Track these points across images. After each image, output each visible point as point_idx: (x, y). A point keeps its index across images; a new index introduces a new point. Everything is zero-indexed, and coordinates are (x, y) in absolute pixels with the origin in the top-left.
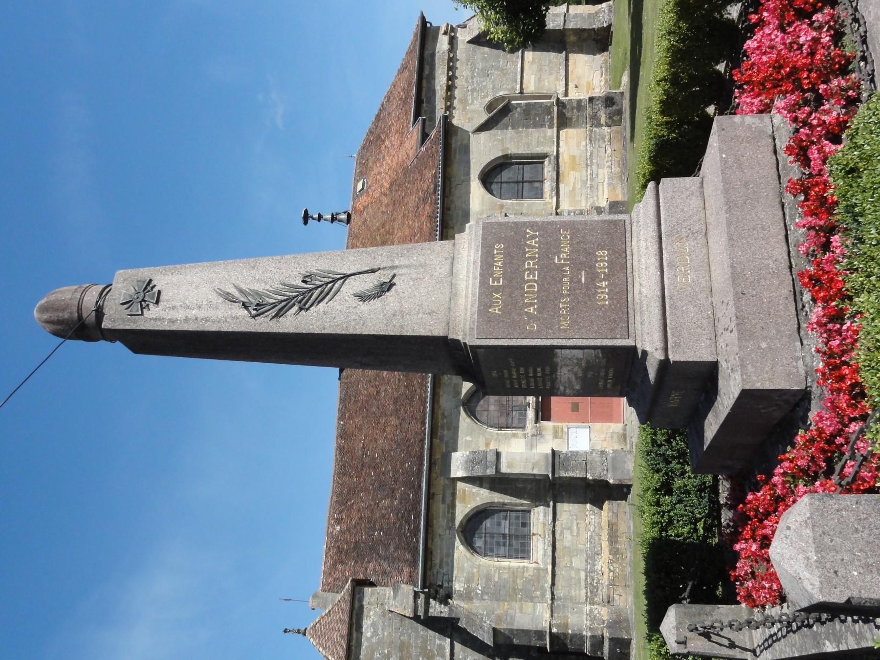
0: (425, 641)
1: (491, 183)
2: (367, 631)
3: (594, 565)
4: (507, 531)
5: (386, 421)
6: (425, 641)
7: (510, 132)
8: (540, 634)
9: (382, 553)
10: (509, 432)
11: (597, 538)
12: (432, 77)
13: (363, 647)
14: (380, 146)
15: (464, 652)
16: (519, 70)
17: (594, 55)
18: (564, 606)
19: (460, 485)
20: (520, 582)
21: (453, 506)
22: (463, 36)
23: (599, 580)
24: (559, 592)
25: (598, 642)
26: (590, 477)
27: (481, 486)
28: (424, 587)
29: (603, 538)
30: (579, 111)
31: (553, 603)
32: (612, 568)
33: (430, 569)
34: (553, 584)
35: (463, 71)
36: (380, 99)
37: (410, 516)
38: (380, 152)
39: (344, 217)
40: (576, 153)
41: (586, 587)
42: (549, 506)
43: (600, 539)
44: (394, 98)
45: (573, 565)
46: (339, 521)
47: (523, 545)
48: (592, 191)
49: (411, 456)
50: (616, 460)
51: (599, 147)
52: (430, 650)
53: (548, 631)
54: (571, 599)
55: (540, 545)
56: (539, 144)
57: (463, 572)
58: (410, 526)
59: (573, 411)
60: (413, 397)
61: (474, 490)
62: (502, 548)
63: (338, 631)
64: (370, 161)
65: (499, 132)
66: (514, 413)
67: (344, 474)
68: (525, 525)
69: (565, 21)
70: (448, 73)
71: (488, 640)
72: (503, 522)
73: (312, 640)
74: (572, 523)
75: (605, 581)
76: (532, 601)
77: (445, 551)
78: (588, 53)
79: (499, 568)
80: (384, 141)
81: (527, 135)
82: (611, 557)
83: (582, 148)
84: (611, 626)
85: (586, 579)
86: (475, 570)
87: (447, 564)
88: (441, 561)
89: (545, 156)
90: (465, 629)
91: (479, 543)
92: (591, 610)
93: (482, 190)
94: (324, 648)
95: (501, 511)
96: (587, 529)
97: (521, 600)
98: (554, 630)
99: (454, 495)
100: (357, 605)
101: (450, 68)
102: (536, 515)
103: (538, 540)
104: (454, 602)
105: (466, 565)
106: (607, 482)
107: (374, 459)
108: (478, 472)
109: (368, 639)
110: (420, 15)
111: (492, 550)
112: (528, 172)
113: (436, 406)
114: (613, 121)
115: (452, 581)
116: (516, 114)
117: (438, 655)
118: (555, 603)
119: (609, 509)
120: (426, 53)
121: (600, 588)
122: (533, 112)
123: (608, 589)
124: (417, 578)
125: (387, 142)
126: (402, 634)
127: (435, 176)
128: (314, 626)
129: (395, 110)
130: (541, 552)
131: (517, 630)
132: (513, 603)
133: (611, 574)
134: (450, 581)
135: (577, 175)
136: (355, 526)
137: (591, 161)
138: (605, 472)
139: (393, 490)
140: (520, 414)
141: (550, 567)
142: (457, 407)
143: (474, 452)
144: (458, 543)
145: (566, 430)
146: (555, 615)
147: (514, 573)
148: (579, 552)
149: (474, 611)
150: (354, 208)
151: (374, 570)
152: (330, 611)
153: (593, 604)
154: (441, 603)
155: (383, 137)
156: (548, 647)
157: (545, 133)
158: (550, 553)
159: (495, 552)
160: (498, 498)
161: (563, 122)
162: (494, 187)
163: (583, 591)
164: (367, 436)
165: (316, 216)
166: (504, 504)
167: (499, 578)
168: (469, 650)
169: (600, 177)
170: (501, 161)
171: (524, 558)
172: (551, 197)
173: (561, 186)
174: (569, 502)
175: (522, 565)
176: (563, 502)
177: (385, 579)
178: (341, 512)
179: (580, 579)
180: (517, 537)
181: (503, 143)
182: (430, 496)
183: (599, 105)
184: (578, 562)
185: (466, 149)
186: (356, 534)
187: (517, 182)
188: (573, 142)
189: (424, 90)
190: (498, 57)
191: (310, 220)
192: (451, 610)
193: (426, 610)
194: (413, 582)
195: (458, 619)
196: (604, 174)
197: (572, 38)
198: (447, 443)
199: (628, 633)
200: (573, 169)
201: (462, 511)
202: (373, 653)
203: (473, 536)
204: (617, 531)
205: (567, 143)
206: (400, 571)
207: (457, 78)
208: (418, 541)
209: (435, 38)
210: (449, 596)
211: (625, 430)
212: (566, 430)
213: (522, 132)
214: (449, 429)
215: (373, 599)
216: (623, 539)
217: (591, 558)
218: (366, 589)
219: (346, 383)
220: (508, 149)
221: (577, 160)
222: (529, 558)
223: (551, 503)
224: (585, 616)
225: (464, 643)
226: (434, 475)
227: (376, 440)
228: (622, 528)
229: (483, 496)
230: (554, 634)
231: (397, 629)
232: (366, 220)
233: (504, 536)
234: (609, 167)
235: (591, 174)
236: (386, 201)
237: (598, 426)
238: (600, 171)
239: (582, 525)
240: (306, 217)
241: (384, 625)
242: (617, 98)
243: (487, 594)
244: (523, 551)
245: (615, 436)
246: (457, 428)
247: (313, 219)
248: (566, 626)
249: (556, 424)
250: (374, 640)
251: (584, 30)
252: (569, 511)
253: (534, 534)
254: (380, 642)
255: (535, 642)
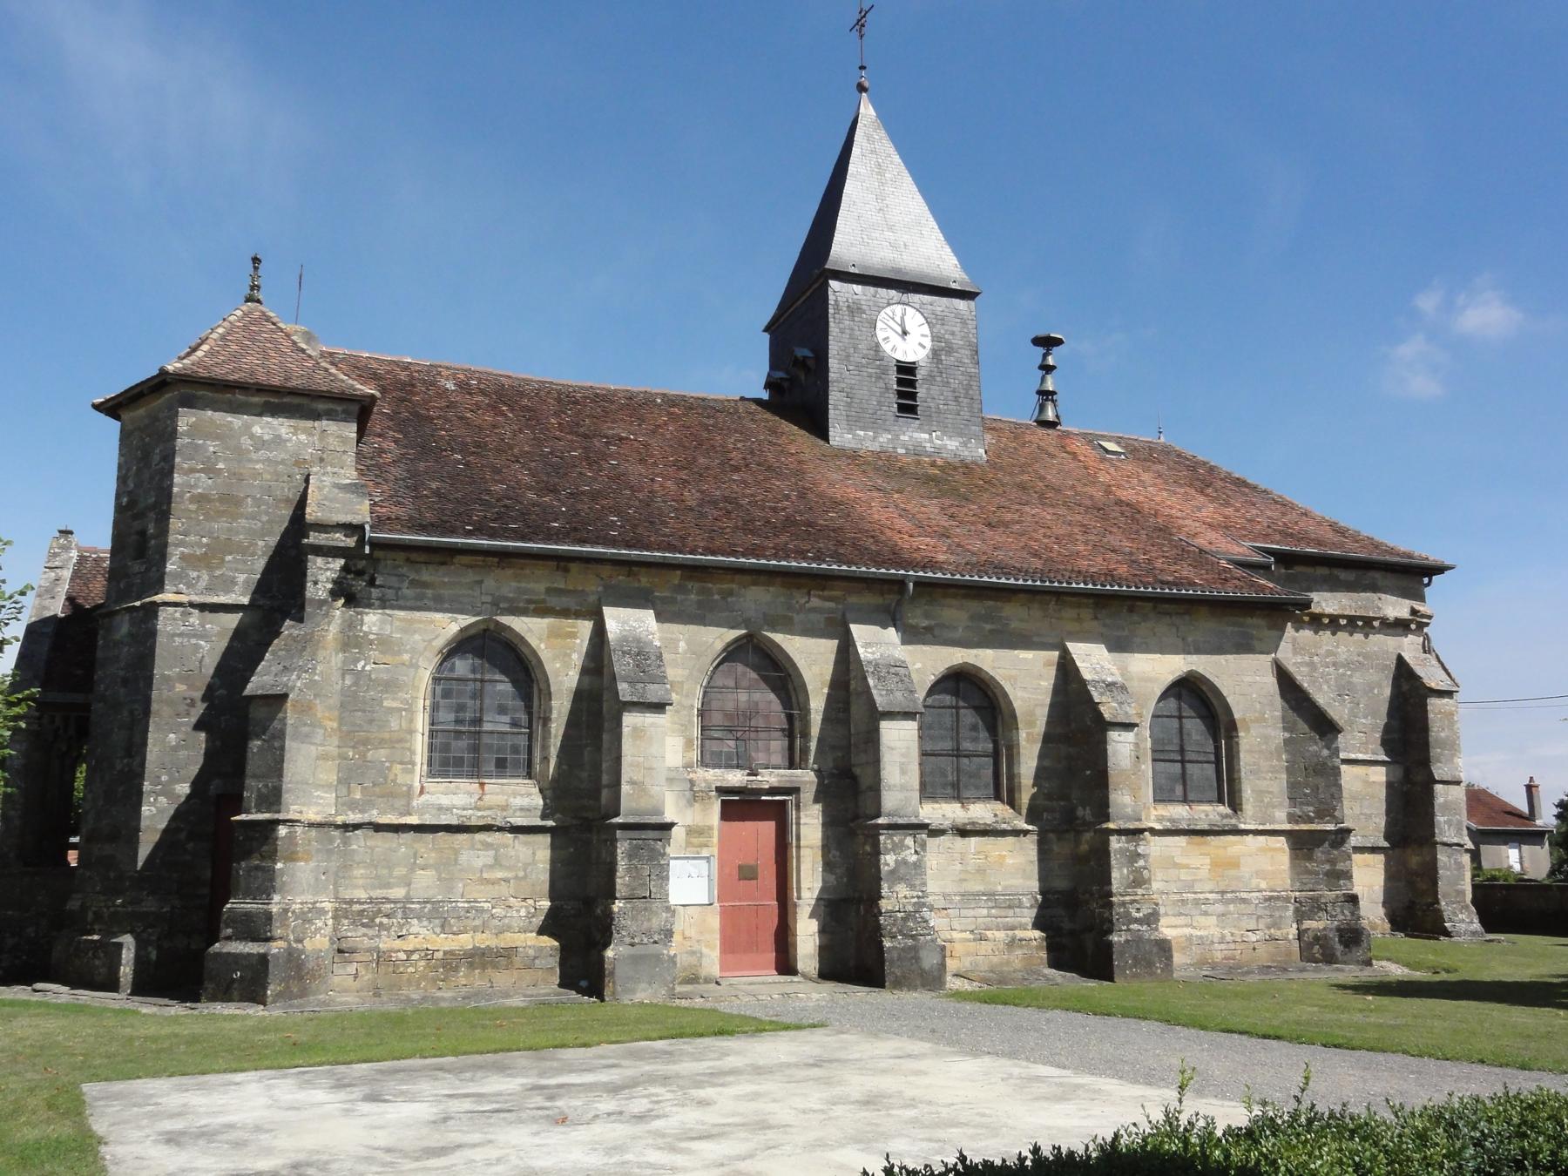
0: (243, 550)
1: (1179, 697)
2: (264, 427)
3: (419, 918)
4: (487, 727)
5: (686, 481)
6: (243, 550)
7: (1279, 735)
8: (273, 798)
9: (422, 466)
10: (696, 732)
11: (478, 922)
12: (1335, 586)
13: (229, 418)
14: (1191, 485)
15: (219, 634)
16: (1353, 756)
17: (1385, 904)
18: (330, 852)
19: (585, 627)
20: (382, 754)
21: (542, 611)
22: (1408, 647)
23: (388, 929)
24: (359, 840)
25: (256, 927)
26: (618, 906)
27: (584, 671)
28: (375, 544)
29: (479, 936)
30: (1328, 874)
31: (337, 827)
32: (415, 957)
33: (408, 560)
34: (378, 828)
35: (1346, 645)
36: (1278, 490)
37: (515, 521)
38: (1181, 486)
39: (1050, 414)
40: (1246, 870)
41: (371, 901)
42: (543, 817)
43: (475, 929)
44: (1284, 514)
45: (418, 872)
46: (463, 387)
47: (459, 762)
48: (1175, 903)
49: (635, 526)
50: (651, 963)
51: (1259, 917)
52: (223, 560)
53: (281, 816)
54: (346, 867)
55: (460, 800)
56: (1259, 793)
57: (405, 631)
58: (494, 520)
59: (740, 867)
60: (753, 532)
61: (575, 656)
62: (452, 717)
63: (263, 366)
64: (1159, 467)
65: (1278, 714)
66: (732, 743)
67: (559, 400)
68: (502, 767)
69: (1450, 845)
70: (1343, 617)
71: (260, 681)
72: (506, 719)
73: (239, 313)
74: (509, 868)
75: (386, 943)
76: (339, 781)
77: (446, 592)
78: (1388, 891)
79: (410, 710)
80: (1202, 492)
81: (1274, 770)
82: (439, 955)
83: (1254, 882)
84: (294, 960)
85: (389, 901)
86: (406, 657)
87: (420, 597)
88: (425, 585)
89: (1236, 806)
90: (277, 634)
91: (462, 666)
92: (322, 912)
93: (1170, 678)
94: (223, 337)
95: (530, 714)
96: (497, 901)
97: (343, 757)
98: (282, 831)
99: (565, 613)
100: (321, 406)
101: (1352, 620)
102: (523, 790)
103: (470, 794)
104: (338, 611)
105: (417, 637)
106: (606, 945)
107: (605, 456)
108: (622, 665)
109: (248, 427)
110: (1447, 563)
111: (447, 694)
112: (1202, 773)
113: (747, 578)
114: (1310, 945)
115: (384, 608)
116: (1317, 748)
117: (212, 577)
118: (336, 833)
119: (541, 949)
120: (1377, 575)
121: (371, 932)
122: (1321, 782)
123: (369, 950)
124: (391, 531)
125: (1202, 499)
126: (258, 502)
127: (1192, 584)
128: (268, 319)
129: (1264, 516)
130: (445, 801)
131: (282, 748)
132: (335, 741)
133: (403, 956)
134: (384, 604)
135: (1204, 873)
136: (461, 418)
137: (1232, 901)
138: (628, 940)
139: (554, 490)
140: (729, 756)
141: (413, 820)
142: (746, 623)
143: (660, 657)
144: (466, 620)
145: (705, 852)
146: (313, 833)
147: (400, 742)
148: (447, 882)
149: (321, 654)
150: (1067, 434)
151: (381, 451)
152: (303, 351)
153: (335, 918)
154: (335, 582)
155: (1209, 491)
156: (243, 817)
157: (1281, 804)
158: (445, 820)
159: (442, 702)
160: (560, 707)
161: (1302, 844)
162: (1172, 703)
163: (363, 895)
164: (646, 445)
165: (1050, 361)
166: (546, 721)
167: (391, 710)
168: (224, 643)
169: (1202, 919)
170: (1223, 718)
171: (430, 764)
172: (1160, 819)
173: (1181, 841)
174: (553, 862)
175: (418, 759)
176: (553, 847)
177: (370, 466)
178: (483, 392)
179: (388, 886)
180: (475, 749)
181: (1257, 720)
182: (562, 562)
183: (1343, 915)
184: (425, 883)
185: (1244, 646)
186: (447, 420)
187: (1182, 751)
188: (1265, 863)
189: (1309, 570)
190: (1374, 715)
191: (1041, 350)
192: (322, 603)
193: (320, 551)
194: (379, 523)
195: (301, 620)
196: (1208, 927)
197: (1414, 860)
198: (673, 601)
199: (279, 996)
200: (1215, 865)
201: (531, 629)
202: (218, 437)
203: (479, 653)
204: (495, 967)
205: (1263, 850)
206: (393, 498)
207: (1334, 634)
208: (469, 534)
209: (1405, 594)
210: (352, 601)
211: (707, 981)
212: (705, 852)
213: (1279, 759)
214: (700, 604)
215: (333, 442)
216: (478, 980)
217: (435, 910)
218: (354, 427)
219: (736, 411)
220: (1248, 730)
221: (1233, 872)
222: (431, 774)
223: (550, 823)
224: (310, 898)
225: (238, 634)
226: (606, 570)
227: (642, 461)
228: (502, 979)
229: (563, 669)
230: (274, 830)
231: (268, 491)
232: (1053, 456)
233: (478, 721)
234: (1223, 937)
235: (1206, 902)
236: (1099, 495)
237: (715, 922)
238: (1213, 920)
239: (504, 890)
240: (1047, 343)
241: (278, 463)
242: (1359, 953)
243: (356, 684)
244: (445, 763)
245: (693, 960)
246: (701, 620)
247: (1045, 356)
248: (291, 858)
249: (716, 833)
250: (246, 442)
251: (1435, 883)
252: (534, 863)
253: (482, 785)
254: (239, 452)
255: (252, 788)
